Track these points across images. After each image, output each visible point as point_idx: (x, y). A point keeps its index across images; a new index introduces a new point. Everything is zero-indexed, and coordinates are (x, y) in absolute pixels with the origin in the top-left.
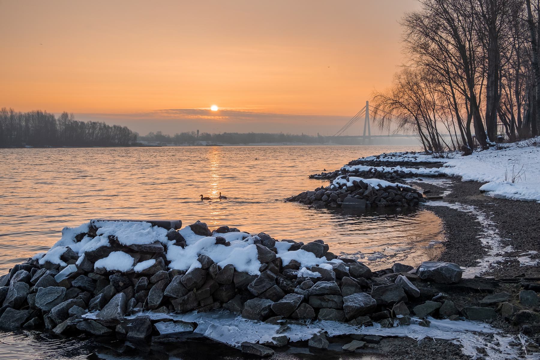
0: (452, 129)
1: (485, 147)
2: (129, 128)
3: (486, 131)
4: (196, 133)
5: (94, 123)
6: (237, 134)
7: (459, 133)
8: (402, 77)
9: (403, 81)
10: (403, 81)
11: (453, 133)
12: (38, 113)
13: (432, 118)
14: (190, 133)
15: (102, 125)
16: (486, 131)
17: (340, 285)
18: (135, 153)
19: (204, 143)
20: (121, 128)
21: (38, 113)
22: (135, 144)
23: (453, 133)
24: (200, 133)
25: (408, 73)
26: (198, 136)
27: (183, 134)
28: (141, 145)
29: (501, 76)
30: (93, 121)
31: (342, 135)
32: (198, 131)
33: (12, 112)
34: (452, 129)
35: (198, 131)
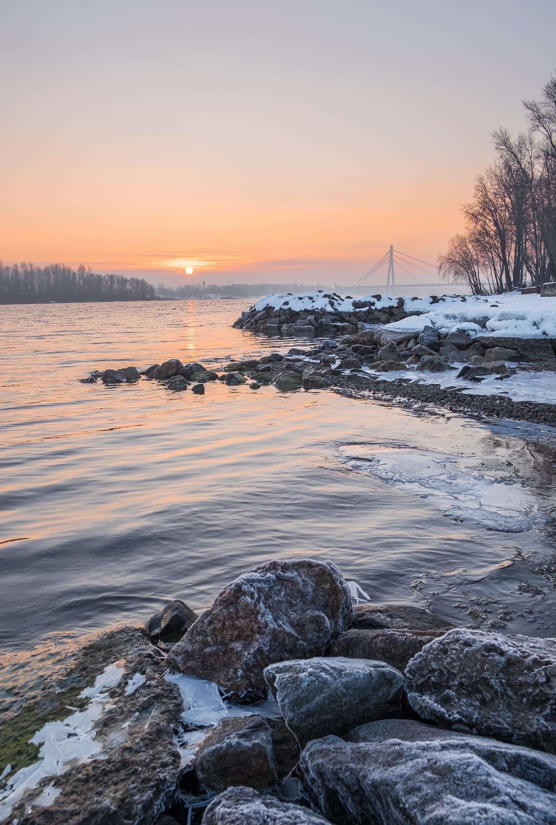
0: (490, 279)
1: (511, 290)
2: (146, 280)
3: (512, 280)
4: (202, 285)
5: (112, 276)
6: (246, 285)
7: (495, 282)
8: (455, 241)
9: (456, 244)
10: (456, 244)
11: (491, 282)
12: (56, 265)
13: (477, 271)
14: (196, 286)
15: (120, 278)
16: (512, 280)
17: (209, 774)
18: (153, 307)
19: (212, 296)
20: (138, 281)
21: (56, 265)
22: (153, 298)
23: (491, 282)
24: (206, 285)
25: (483, 440)
26: (204, 289)
27: (186, 286)
28: (159, 299)
29: (526, 240)
30: (110, 274)
31: (362, 285)
32: (204, 283)
33: (31, 265)
34: (490, 279)
35: (204, 283)
